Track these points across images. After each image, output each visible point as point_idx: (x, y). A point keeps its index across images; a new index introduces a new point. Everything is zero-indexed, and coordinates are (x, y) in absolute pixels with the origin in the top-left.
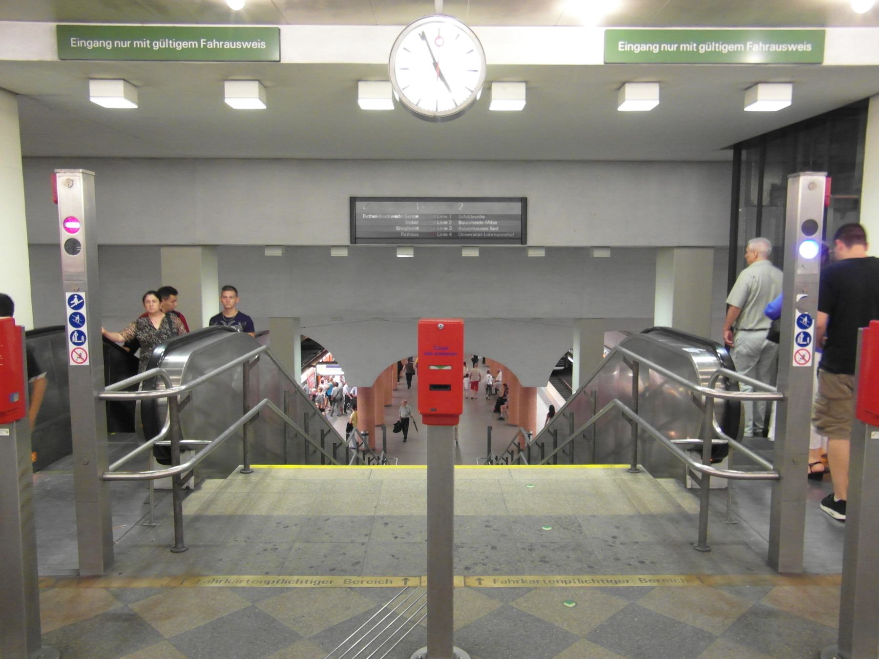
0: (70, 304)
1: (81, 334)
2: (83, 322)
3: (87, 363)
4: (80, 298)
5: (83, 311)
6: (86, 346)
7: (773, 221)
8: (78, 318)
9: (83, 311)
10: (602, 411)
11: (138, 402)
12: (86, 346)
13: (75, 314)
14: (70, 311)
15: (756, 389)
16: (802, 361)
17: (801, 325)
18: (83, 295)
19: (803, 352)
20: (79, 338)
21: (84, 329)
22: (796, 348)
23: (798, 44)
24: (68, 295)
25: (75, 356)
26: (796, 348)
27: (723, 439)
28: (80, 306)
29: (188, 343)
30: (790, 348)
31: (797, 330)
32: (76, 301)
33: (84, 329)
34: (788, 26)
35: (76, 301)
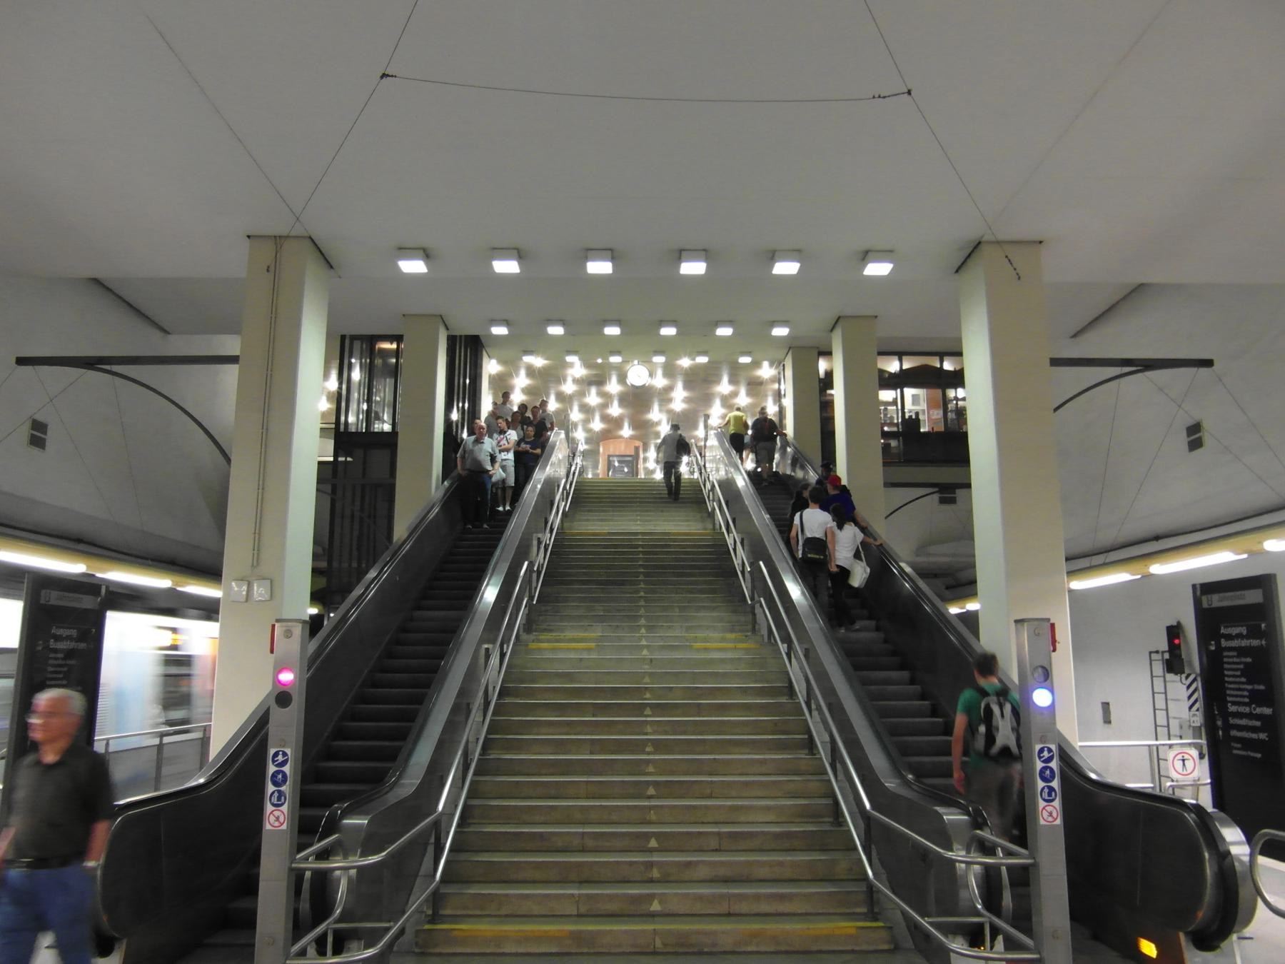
0: (274, 761)
1: (1051, 789)
2: (1053, 777)
3: (284, 827)
4: (285, 754)
6: (285, 808)
8: (1048, 772)
9: (287, 769)
11: (308, 874)
12: (285, 808)
13: (277, 772)
14: (1039, 765)
15: (1009, 854)
16: (277, 824)
18: (288, 751)
19: (277, 813)
20: (1050, 795)
22: (1042, 804)
23: (790, 477)
24: (1038, 747)
25: (1045, 814)
26: (1042, 804)
27: (986, 918)
29: (1027, 802)
30: (1035, 804)
31: (1041, 784)
32: (1046, 754)
35: (1046, 754)
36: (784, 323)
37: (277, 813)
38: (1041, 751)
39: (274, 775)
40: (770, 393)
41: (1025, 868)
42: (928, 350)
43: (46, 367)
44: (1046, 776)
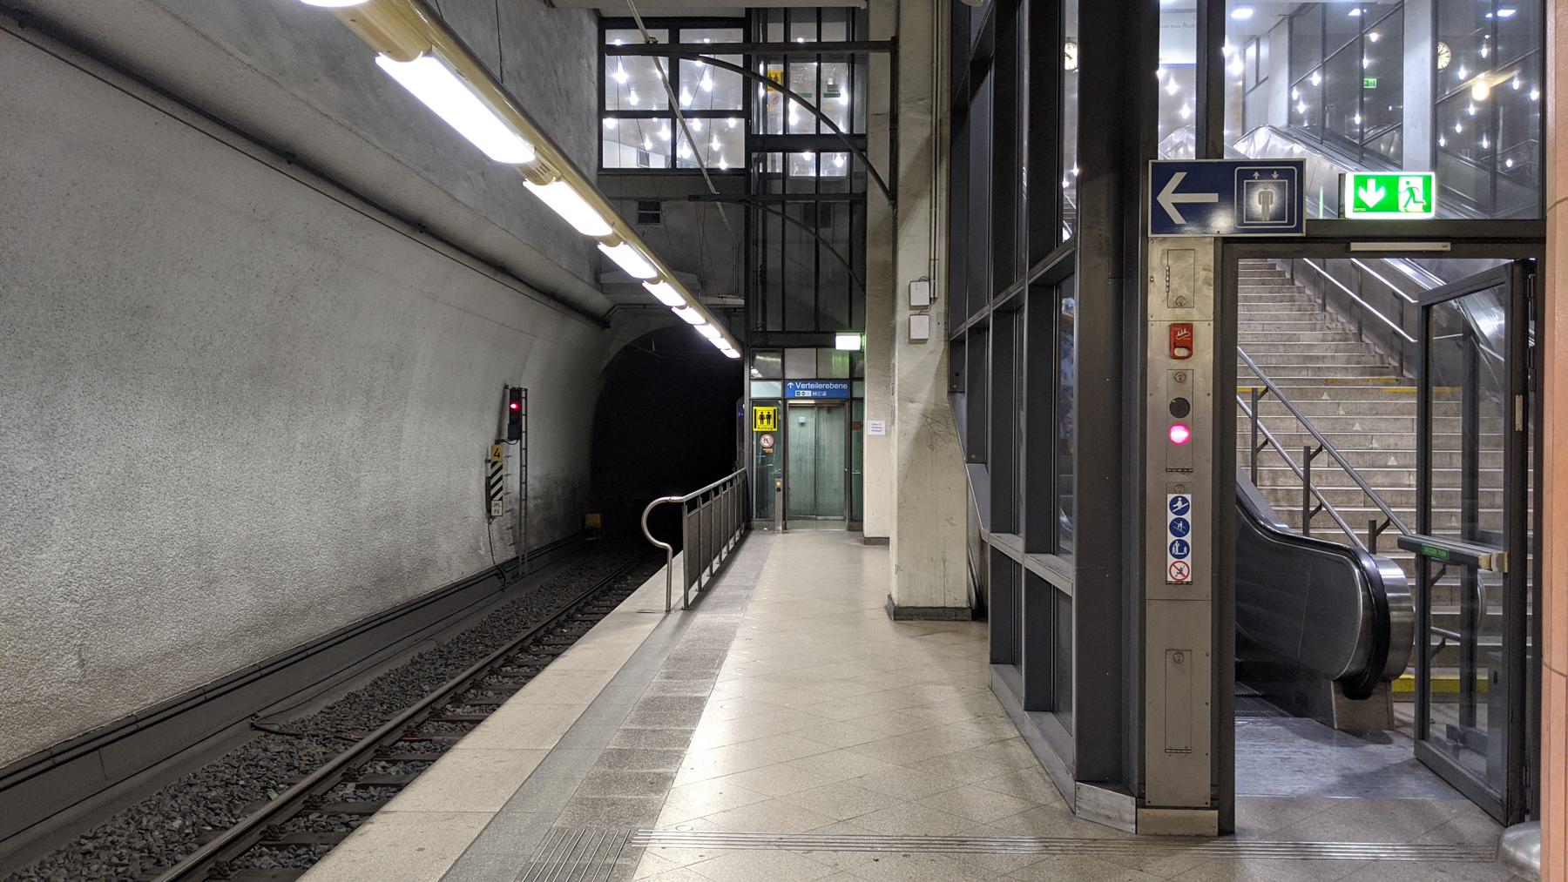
1: (1183, 544)
4: (1184, 500)
5: (1188, 517)
6: (1188, 560)
7: (1456, 404)
9: (1188, 517)
10: (402, 662)
12: (1188, 560)
13: (1178, 520)
14: (1171, 517)
17: (1175, 533)
18: (1188, 497)
19: (1179, 565)
20: (1181, 550)
21: (1188, 538)
22: (1171, 559)
24: (1170, 497)
26: (1171, 559)
28: (1184, 511)
31: (1171, 538)
32: (1179, 505)
33: (1188, 538)
34: (1031, 115)
36: (1507, 6)
37: (1179, 565)
38: (1175, 500)
39: (1173, 524)
40: (1500, 80)
41: (996, 528)
42: (1538, 9)
43: (455, 578)
44: (1179, 528)
